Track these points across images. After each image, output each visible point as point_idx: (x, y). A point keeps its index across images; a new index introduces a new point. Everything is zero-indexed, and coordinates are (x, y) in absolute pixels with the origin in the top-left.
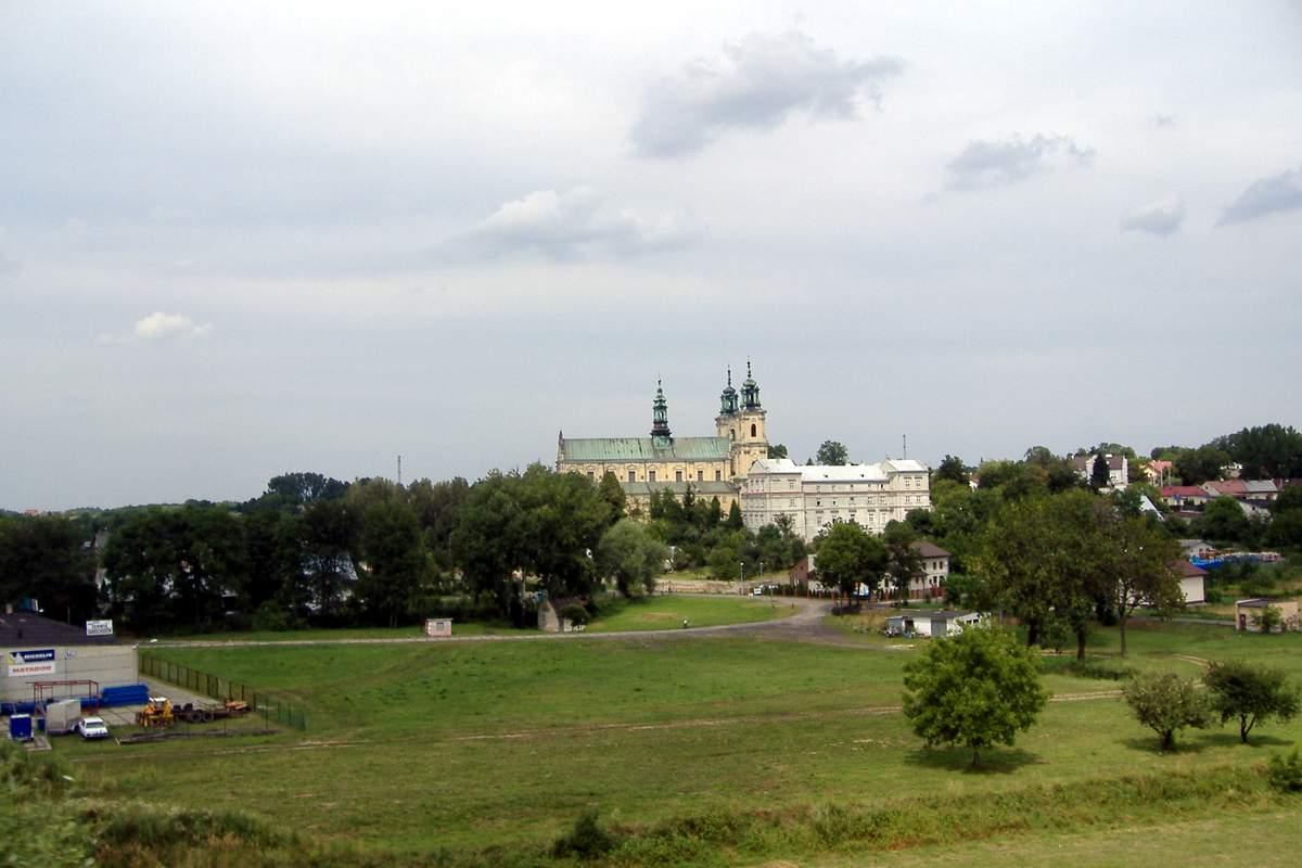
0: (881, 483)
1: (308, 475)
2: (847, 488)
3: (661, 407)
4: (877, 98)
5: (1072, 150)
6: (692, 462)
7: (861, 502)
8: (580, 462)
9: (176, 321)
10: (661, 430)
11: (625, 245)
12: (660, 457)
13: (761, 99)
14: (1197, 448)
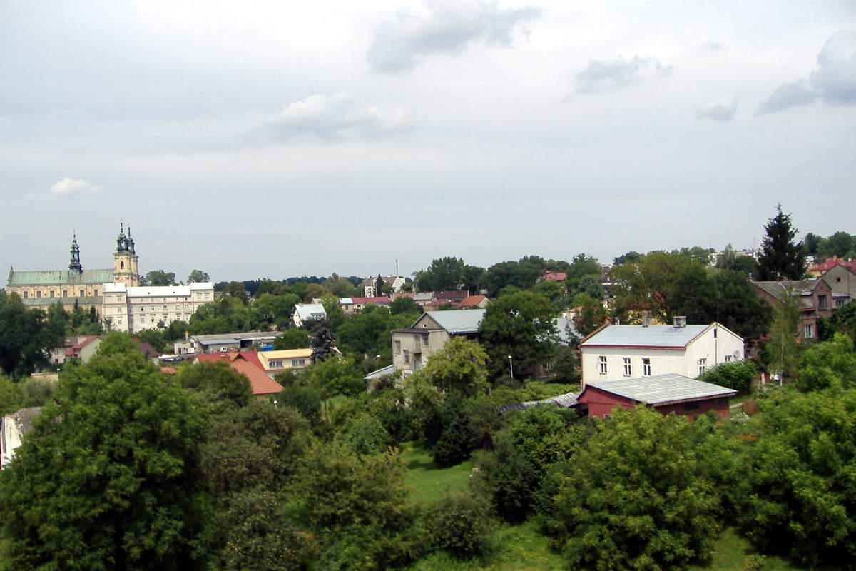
0: (186, 297)
1: (445, 259)
2: (162, 300)
3: (75, 251)
4: (527, 33)
5: (658, 66)
6: (90, 284)
7: (171, 309)
8: (19, 286)
9: (79, 184)
10: (76, 266)
11: (371, 131)
12: (71, 282)
13: (448, 38)
14: (275, 280)
